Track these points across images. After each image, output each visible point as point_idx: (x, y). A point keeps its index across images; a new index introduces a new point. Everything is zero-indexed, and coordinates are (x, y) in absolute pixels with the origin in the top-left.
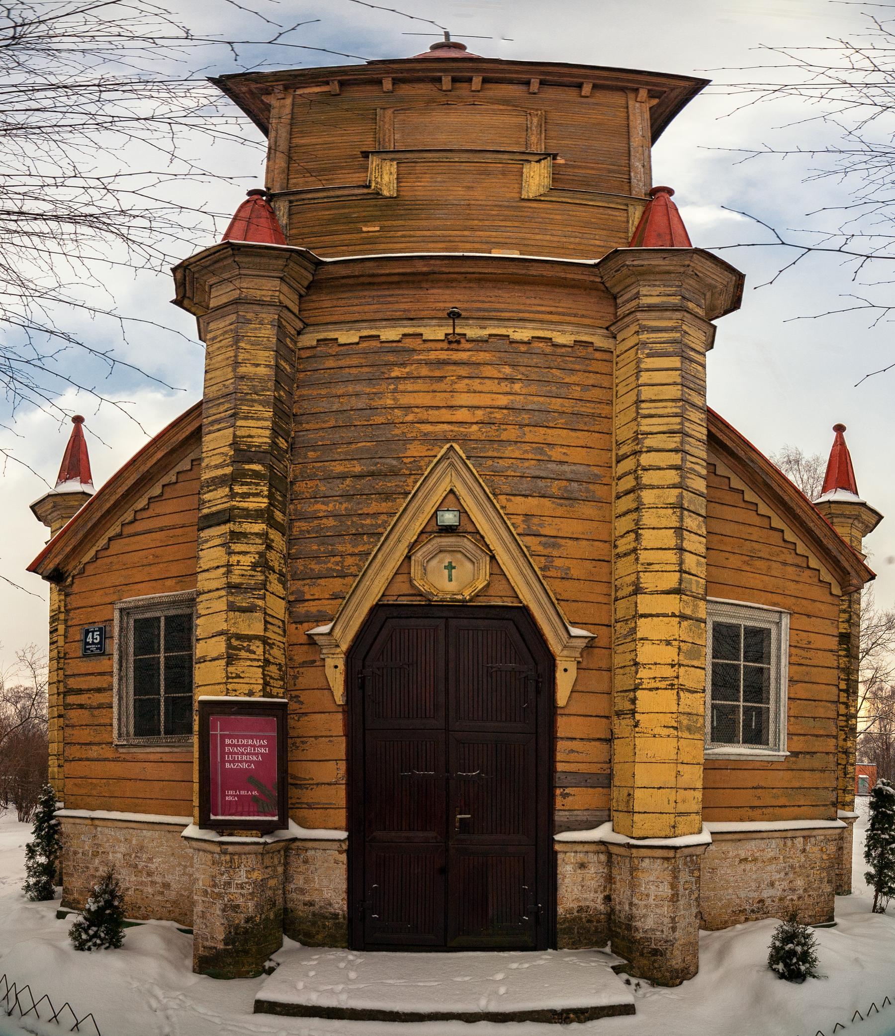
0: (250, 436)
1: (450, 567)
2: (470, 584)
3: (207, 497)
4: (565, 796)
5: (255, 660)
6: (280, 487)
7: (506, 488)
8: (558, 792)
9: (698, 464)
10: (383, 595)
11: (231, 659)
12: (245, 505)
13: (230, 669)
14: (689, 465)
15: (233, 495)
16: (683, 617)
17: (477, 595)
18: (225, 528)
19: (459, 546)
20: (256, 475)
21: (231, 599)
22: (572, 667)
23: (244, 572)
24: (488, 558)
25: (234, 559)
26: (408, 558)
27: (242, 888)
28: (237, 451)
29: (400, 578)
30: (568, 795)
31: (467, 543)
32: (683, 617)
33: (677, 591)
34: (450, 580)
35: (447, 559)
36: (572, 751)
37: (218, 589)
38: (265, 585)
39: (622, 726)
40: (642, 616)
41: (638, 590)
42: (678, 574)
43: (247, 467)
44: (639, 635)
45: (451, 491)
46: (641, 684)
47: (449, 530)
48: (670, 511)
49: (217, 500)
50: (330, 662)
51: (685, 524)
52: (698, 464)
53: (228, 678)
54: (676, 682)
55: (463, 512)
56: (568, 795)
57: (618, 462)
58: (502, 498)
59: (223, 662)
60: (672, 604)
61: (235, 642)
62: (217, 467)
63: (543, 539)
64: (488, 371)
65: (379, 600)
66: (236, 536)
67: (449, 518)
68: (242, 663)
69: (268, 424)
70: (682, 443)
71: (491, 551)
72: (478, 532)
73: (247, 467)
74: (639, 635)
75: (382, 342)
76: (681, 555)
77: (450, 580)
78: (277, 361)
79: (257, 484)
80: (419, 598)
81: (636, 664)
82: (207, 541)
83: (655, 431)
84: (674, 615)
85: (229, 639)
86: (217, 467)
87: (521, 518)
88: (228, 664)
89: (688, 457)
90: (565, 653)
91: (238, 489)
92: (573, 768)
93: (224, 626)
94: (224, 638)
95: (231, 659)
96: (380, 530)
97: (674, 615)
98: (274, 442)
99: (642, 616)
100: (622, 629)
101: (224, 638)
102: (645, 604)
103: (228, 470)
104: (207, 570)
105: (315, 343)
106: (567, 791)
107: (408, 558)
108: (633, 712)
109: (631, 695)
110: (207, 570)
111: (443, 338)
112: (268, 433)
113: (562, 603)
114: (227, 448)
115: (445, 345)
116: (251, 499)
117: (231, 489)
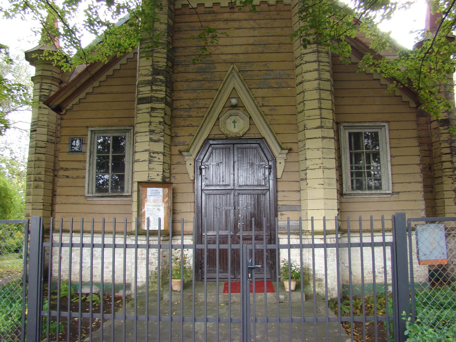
0: (158, 62)
1: (234, 122)
2: (242, 130)
3: (141, 89)
4: (282, 215)
5: (160, 162)
6: (170, 85)
7: (255, 86)
8: (279, 213)
9: (325, 66)
10: (209, 135)
11: (150, 162)
12: (156, 95)
13: (150, 165)
14: (321, 67)
15: (152, 90)
16: (323, 138)
17: (245, 134)
18: (149, 105)
19: (238, 113)
20: (161, 80)
21: (151, 136)
22: (283, 162)
23: (156, 125)
24: (249, 118)
25: (153, 119)
26: (218, 119)
27: (154, 255)
28: (154, 69)
29: (215, 127)
30: (283, 214)
31: (240, 112)
32: (323, 138)
33: (321, 127)
34: (235, 127)
35: (233, 118)
36: (284, 196)
37: (145, 132)
38: (164, 131)
39: (303, 183)
40: (308, 139)
41: (305, 128)
42: (320, 119)
43: (157, 77)
44: (307, 147)
45: (234, 88)
46: (308, 167)
47: (234, 107)
48: (315, 91)
49: (145, 91)
50: (188, 163)
51: (321, 97)
52: (325, 66)
53: (149, 169)
54: (321, 165)
55: (238, 98)
56: (283, 214)
57: (296, 68)
58: (253, 90)
59: (147, 163)
60: (318, 133)
61: (152, 154)
62: (145, 75)
63: (270, 107)
64: (245, 24)
65: (208, 137)
66: (153, 109)
67: (234, 101)
68: (155, 163)
69: (165, 56)
70: (318, 57)
71: (250, 115)
72: (244, 107)
73: (157, 77)
74: (307, 147)
75: (206, 8)
76: (321, 111)
77: (235, 127)
78: (168, 21)
79: (161, 86)
80: (223, 136)
81: (306, 159)
82: (140, 110)
83: (307, 52)
84: (319, 138)
85: (150, 153)
86: (145, 75)
87: (261, 98)
88: (149, 163)
89: (321, 63)
90: (280, 156)
91: (154, 88)
92: (284, 203)
93: (148, 148)
94: (148, 153)
95: (150, 162)
96: (207, 106)
97: (319, 138)
98: (167, 65)
99: (308, 139)
100: (300, 108)
101: (148, 153)
102: (309, 134)
103: (150, 78)
104: (141, 123)
105: (180, 7)
106: (283, 213)
107: (218, 119)
108: (306, 179)
109: (305, 172)
110: (141, 123)
111: (227, 5)
112: (165, 60)
113: (278, 135)
114: (150, 67)
115: (228, 10)
116: (159, 92)
117: (151, 88)
